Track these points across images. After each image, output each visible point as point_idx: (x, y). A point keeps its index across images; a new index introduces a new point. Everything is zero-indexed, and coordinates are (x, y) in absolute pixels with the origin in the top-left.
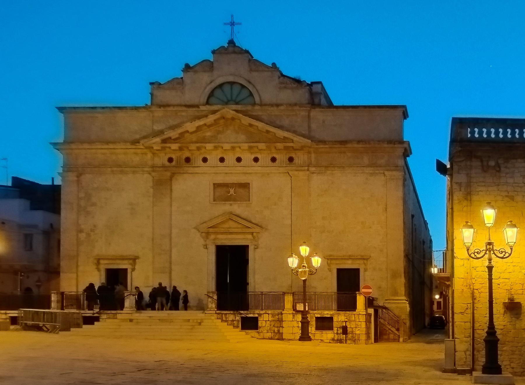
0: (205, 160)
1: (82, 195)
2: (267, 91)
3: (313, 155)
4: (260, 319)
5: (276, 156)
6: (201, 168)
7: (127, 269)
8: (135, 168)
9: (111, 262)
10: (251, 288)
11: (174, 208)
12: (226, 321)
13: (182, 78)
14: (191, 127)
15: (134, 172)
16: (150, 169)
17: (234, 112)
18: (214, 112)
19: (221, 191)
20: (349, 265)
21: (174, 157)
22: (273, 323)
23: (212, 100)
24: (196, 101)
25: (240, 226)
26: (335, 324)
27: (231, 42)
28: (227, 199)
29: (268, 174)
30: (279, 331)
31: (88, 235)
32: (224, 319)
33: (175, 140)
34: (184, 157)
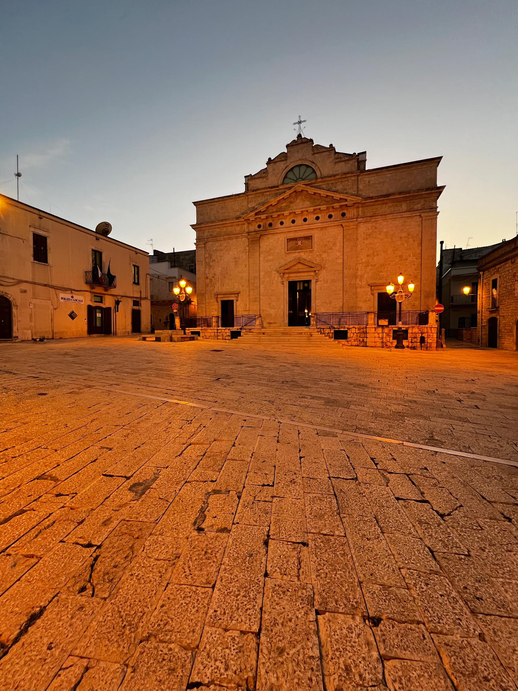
0: (282, 223)
1: (207, 255)
2: (326, 167)
4: (349, 332)
5: (333, 214)
6: (279, 229)
7: (233, 301)
8: (237, 236)
9: (224, 296)
11: (261, 259)
12: (324, 333)
13: (266, 168)
15: (237, 238)
16: (246, 234)
17: (304, 186)
18: (290, 188)
21: (261, 224)
22: (359, 335)
23: (286, 180)
24: (275, 184)
25: (305, 267)
27: (299, 136)
28: (297, 248)
29: (326, 227)
30: (363, 340)
31: (211, 280)
32: (322, 332)
33: (263, 213)
34: (268, 223)
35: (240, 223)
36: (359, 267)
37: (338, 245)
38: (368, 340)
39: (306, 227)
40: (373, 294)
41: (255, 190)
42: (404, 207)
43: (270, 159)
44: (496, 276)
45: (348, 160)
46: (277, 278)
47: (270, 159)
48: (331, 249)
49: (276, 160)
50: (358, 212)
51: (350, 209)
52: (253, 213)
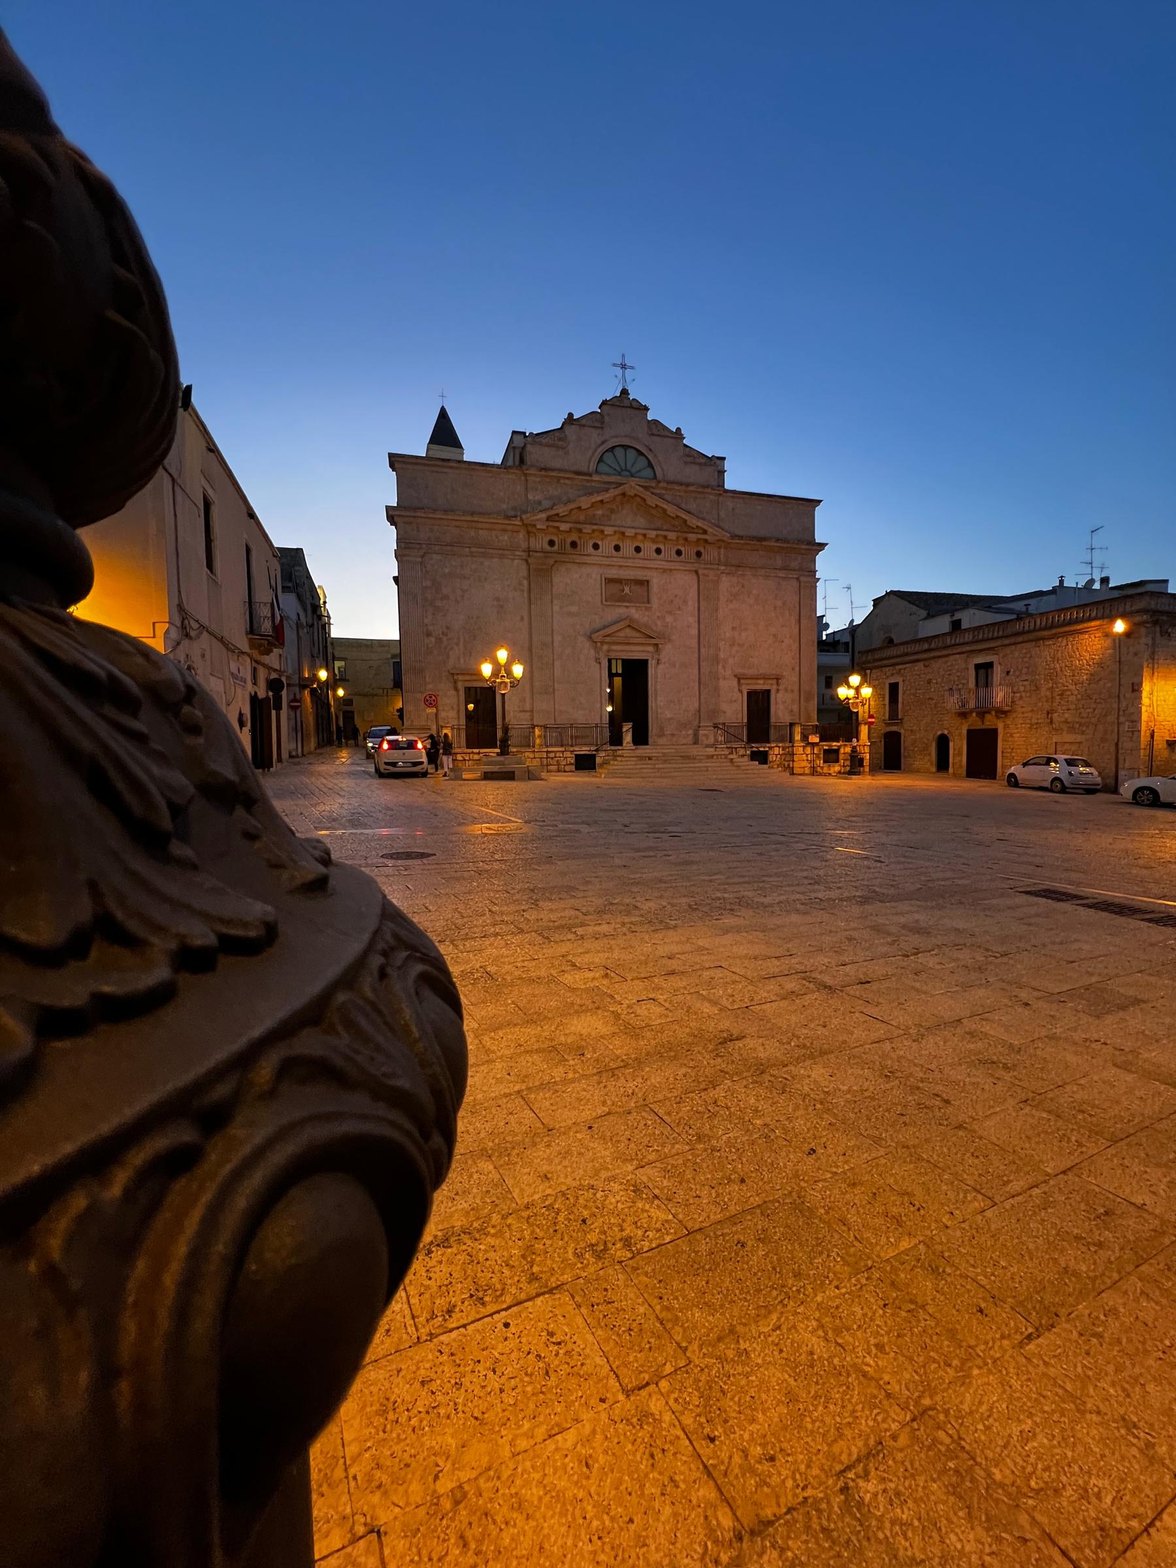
0: (596, 547)
2: (670, 468)
3: (722, 551)
4: (771, 752)
5: (682, 549)
10: (773, 720)
14: (585, 502)
15: (502, 557)
19: (615, 588)
20: (760, 686)
25: (638, 635)
26: (841, 757)
27: (625, 392)
28: (623, 599)
31: (439, 640)
35: (510, 528)
36: (721, 644)
37: (690, 603)
38: (796, 764)
39: (640, 563)
40: (741, 691)
41: (545, 469)
42: (779, 562)
43: (571, 415)
44: (899, 679)
45: (705, 464)
46: (588, 651)
47: (571, 415)
48: (679, 609)
49: (584, 422)
50: (719, 554)
51: (709, 547)
52: (543, 516)
